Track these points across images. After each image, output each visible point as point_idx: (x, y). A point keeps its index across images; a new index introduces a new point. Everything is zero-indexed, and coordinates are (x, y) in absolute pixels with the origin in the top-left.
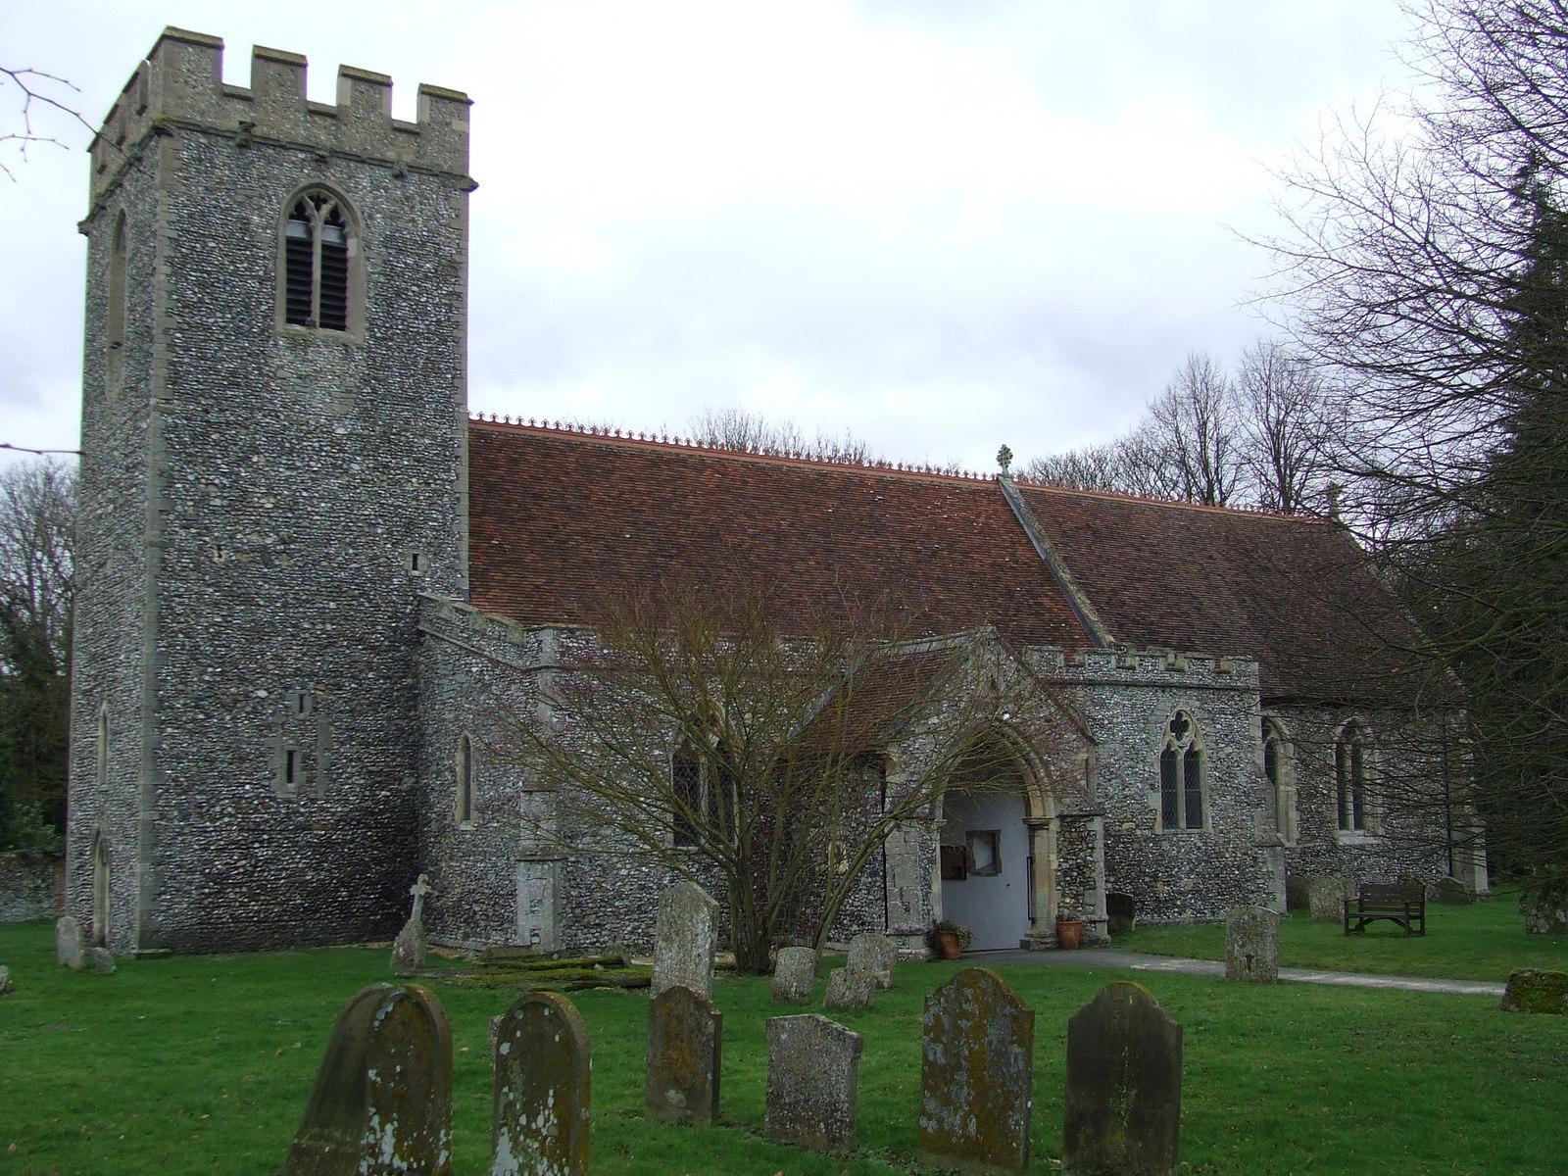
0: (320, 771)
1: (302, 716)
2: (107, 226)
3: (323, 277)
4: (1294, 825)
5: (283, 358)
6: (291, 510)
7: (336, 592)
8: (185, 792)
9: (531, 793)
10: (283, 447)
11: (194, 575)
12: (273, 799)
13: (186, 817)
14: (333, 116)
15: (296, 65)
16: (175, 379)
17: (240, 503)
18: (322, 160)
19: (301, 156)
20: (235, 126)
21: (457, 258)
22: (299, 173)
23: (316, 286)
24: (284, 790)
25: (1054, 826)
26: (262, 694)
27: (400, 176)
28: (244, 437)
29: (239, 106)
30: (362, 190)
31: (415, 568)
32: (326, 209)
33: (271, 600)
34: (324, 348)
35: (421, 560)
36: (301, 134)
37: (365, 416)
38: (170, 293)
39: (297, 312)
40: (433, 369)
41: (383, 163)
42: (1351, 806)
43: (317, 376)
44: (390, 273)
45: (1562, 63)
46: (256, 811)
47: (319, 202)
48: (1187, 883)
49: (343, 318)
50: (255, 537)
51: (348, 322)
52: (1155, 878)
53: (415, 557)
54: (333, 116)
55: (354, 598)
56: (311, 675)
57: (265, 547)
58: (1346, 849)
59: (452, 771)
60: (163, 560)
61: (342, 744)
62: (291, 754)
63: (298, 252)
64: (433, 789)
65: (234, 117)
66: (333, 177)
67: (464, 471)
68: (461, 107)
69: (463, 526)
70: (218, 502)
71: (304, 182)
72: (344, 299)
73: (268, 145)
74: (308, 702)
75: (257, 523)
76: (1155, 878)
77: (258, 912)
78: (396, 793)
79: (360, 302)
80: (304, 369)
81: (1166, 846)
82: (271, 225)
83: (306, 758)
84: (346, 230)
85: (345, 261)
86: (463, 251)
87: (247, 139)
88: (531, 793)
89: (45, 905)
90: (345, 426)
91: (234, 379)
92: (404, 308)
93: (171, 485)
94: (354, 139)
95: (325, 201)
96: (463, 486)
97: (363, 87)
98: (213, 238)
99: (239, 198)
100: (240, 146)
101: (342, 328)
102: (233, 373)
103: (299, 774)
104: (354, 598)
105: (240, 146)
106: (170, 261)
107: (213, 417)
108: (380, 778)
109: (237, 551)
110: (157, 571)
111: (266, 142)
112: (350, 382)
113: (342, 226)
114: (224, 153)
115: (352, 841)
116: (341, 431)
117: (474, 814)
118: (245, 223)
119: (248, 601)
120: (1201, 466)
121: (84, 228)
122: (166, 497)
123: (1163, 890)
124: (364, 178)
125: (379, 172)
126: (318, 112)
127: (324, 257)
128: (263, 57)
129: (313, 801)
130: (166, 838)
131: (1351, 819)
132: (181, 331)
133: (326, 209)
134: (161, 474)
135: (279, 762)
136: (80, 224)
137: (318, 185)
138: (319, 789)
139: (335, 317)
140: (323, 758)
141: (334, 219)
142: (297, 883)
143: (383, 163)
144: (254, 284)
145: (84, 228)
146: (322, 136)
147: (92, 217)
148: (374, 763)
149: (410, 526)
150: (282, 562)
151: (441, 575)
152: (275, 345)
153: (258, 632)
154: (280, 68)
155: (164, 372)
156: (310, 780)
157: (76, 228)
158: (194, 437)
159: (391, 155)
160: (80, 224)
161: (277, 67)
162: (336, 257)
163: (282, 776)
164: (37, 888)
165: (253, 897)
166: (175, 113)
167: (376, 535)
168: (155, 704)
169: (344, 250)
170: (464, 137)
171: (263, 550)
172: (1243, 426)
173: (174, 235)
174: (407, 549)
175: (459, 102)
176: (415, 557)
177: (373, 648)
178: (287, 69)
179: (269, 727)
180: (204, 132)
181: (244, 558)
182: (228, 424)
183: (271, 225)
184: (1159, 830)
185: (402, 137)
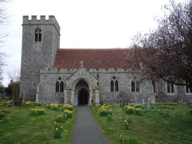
4: (176, 92)
5: (34, 45)
15: (36, 16)
17: (29, 60)
18: (38, 25)
24: (33, 87)
25: (92, 91)
27: (46, 25)
28: (30, 53)
30: (42, 28)
34: (39, 44)
37: (42, 50)
39: (36, 40)
45: (1, 14)
47: (38, 29)
48: (136, 99)
52: (130, 98)
58: (187, 95)
66: (39, 27)
68: (43, 18)
71: (36, 28)
76: (130, 98)
79: (42, 39)
80: (36, 46)
81: (132, 94)
82: (39, 32)
92: (46, 39)
94: (41, 23)
103: (35, 85)
118: (30, 33)
119: (30, 69)
123: (131, 100)
124: (42, 26)
128: (32, 16)
135: (33, 84)
139: (40, 40)
143: (44, 24)
144: (31, 38)
149: (47, 60)
150: (34, 65)
153: (31, 72)
154: (34, 17)
159: (45, 23)
162: (40, 35)
171: (32, 64)
172: (171, 30)
175: (53, 16)
183: (39, 32)
184: (131, 92)
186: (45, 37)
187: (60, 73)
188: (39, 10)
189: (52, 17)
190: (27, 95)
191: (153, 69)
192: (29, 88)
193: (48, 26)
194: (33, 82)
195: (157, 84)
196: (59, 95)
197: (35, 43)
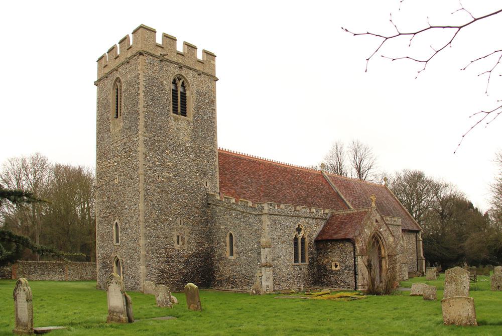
0: (186, 242)
1: (180, 226)
2: (109, 83)
3: (181, 101)
6: (176, 167)
7: (187, 191)
8: (153, 246)
9: (264, 248)
10: (173, 149)
11: (153, 184)
12: (175, 249)
13: (153, 254)
14: (183, 55)
16: (146, 127)
17: (163, 164)
19: (176, 65)
20: (159, 55)
21: (214, 99)
22: (174, 71)
23: (180, 104)
26: (171, 219)
27: (199, 75)
29: (160, 49)
30: (190, 76)
31: (206, 186)
32: (181, 81)
33: (172, 192)
35: (208, 184)
36: (175, 60)
38: (144, 101)
39: (175, 111)
40: (208, 130)
41: (195, 70)
42: (300, 256)
43: (181, 129)
44: (198, 101)
46: (170, 252)
47: (180, 79)
49: (186, 113)
50: (167, 174)
51: (187, 114)
53: (206, 182)
54: (183, 55)
55: (192, 193)
56: (182, 214)
57: (170, 177)
59: (225, 242)
60: (145, 179)
61: (191, 234)
62: (178, 237)
63: (175, 92)
64: (216, 247)
65: (159, 52)
66: (183, 72)
67: (217, 159)
69: (217, 175)
70: (158, 163)
71: (176, 73)
72: (186, 108)
73: (167, 61)
74: (182, 222)
75: (168, 170)
77: (172, 280)
78: (204, 248)
82: (155, 87)
83: (182, 238)
84: (186, 88)
85: (186, 97)
86: (215, 97)
87: (162, 59)
88: (264, 248)
89: (63, 276)
90: (188, 144)
91: (161, 128)
93: (146, 157)
95: (181, 79)
96: (217, 163)
97: (190, 48)
98: (155, 86)
99: (161, 76)
100: (161, 61)
101: (186, 116)
102: (161, 126)
103: (181, 243)
104: (192, 193)
105: (161, 61)
106: (144, 92)
107: (156, 138)
108: (200, 244)
109: (163, 177)
110: (144, 182)
111: (167, 60)
112: (189, 132)
113: (185, 87)
114: (157, 62)
115: (194, 261)
116: (187, 145)
117: (235, 254)
118: (162, 83)
119: (166, 192)
120: (338, 169)
121: (96, 84)
122: (145, 160)
125: (194, 73)
126: (179, 53)
127: (181, 96)
129: (184, 250)
130: (148, 259)
131: (300, 259)
132: (147, 112)
133: (181, 81)
134: (144, 153)
136: (95, 82)
137: (179, 74)
138: (186, 246)
139: (184, 113)
140: (186, 238)
141: (183, 85)
142: (181, 273)
145: (96, 84)
146: (180, 60)
147: (99, 80)
148: (198, 240)
149: (205, 174)
151: (212, 186)
152: (171, 119)
153: (169, 202)
154: (170, 39)
155: (143, 124)
156: (183, 244)
157: (94, 83)
158: (151, 143)
159: (197, 68)
160: (95, 82)
161: (169, 39)
163: (176, 243)
164: (61, 271)
165: (171, 276)
166: (145, 49)
167: (197, 176)
168: (144, 221)
169: (185, 94)
170: (214, 65)
173: (145, 84)
174: (205, 180)
176: (206, 182)
177: (197, 208)
178: (171, 40)
179: (173, 229)
180: (152, 56)
181: (165, 180)
182: (160, 140)
183: (155, 87)
185: (200, 63)
186: (198, 109)
187: (299, 217)
188: (184, 24)
189: (210, 55)
190: (162, 271)
191: (33, 234)
192: (165, 249)
193: (202, 78)
194: (175, 233)
195: (363, 258)
196: (301, 269)
197: (176, 120)
